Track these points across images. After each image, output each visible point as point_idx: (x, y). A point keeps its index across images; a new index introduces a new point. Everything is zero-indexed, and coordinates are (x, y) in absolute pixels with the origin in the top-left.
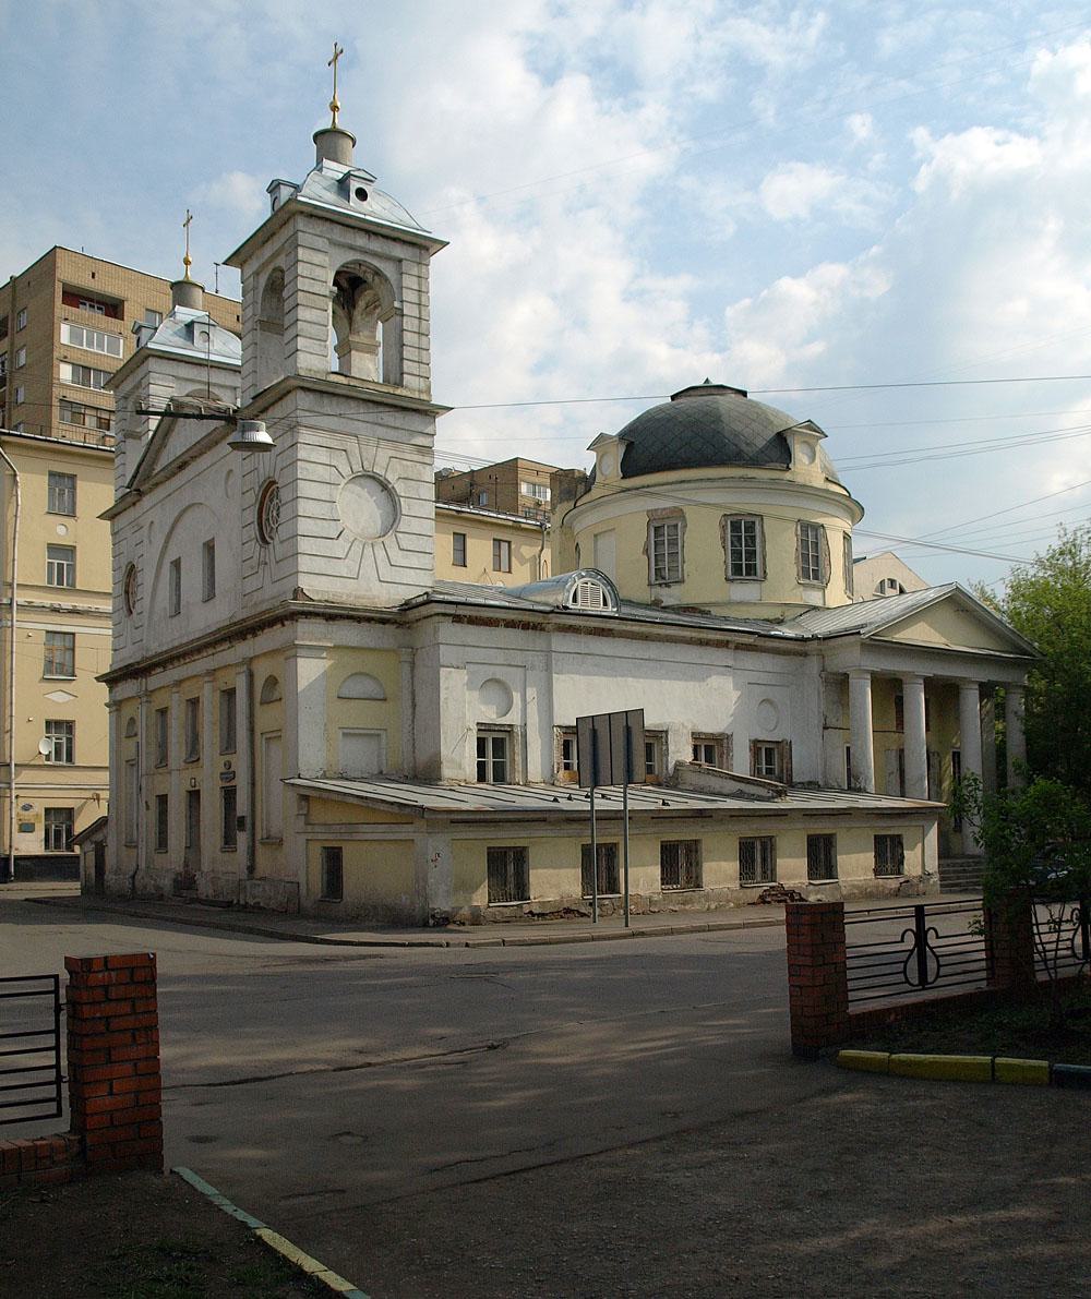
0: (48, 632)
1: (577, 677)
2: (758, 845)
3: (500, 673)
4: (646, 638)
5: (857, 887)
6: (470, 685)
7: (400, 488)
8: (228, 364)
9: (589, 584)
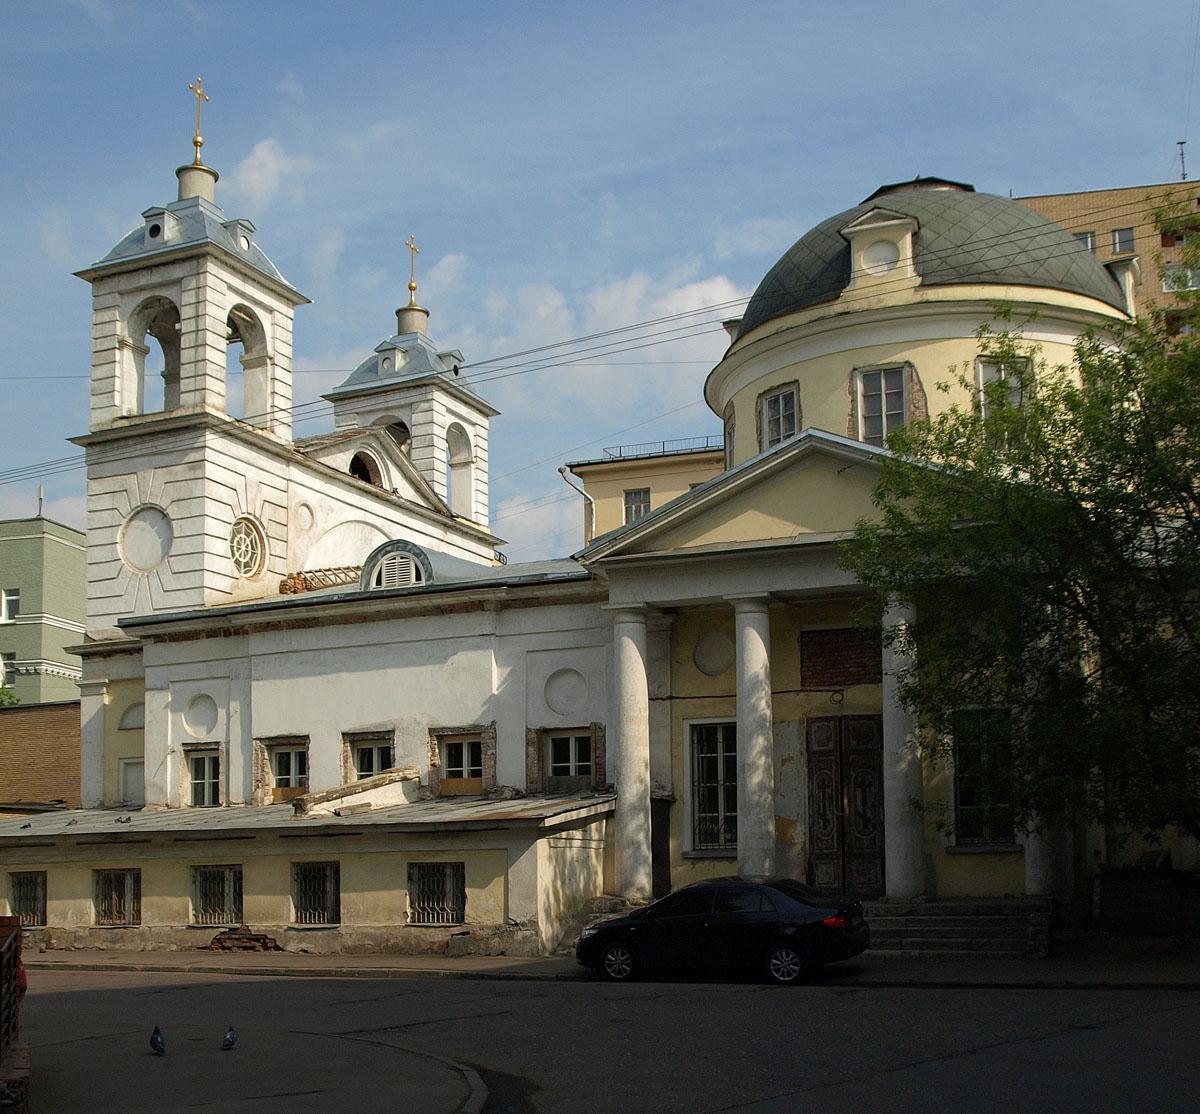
1: (278, 682)
2: (229, 875)
3: (205, 687)
4: (364, 619)
5: (371, 937)
6: (174, 707)
7: (172, 512)
8: (363, 390)
9: (398, 560)
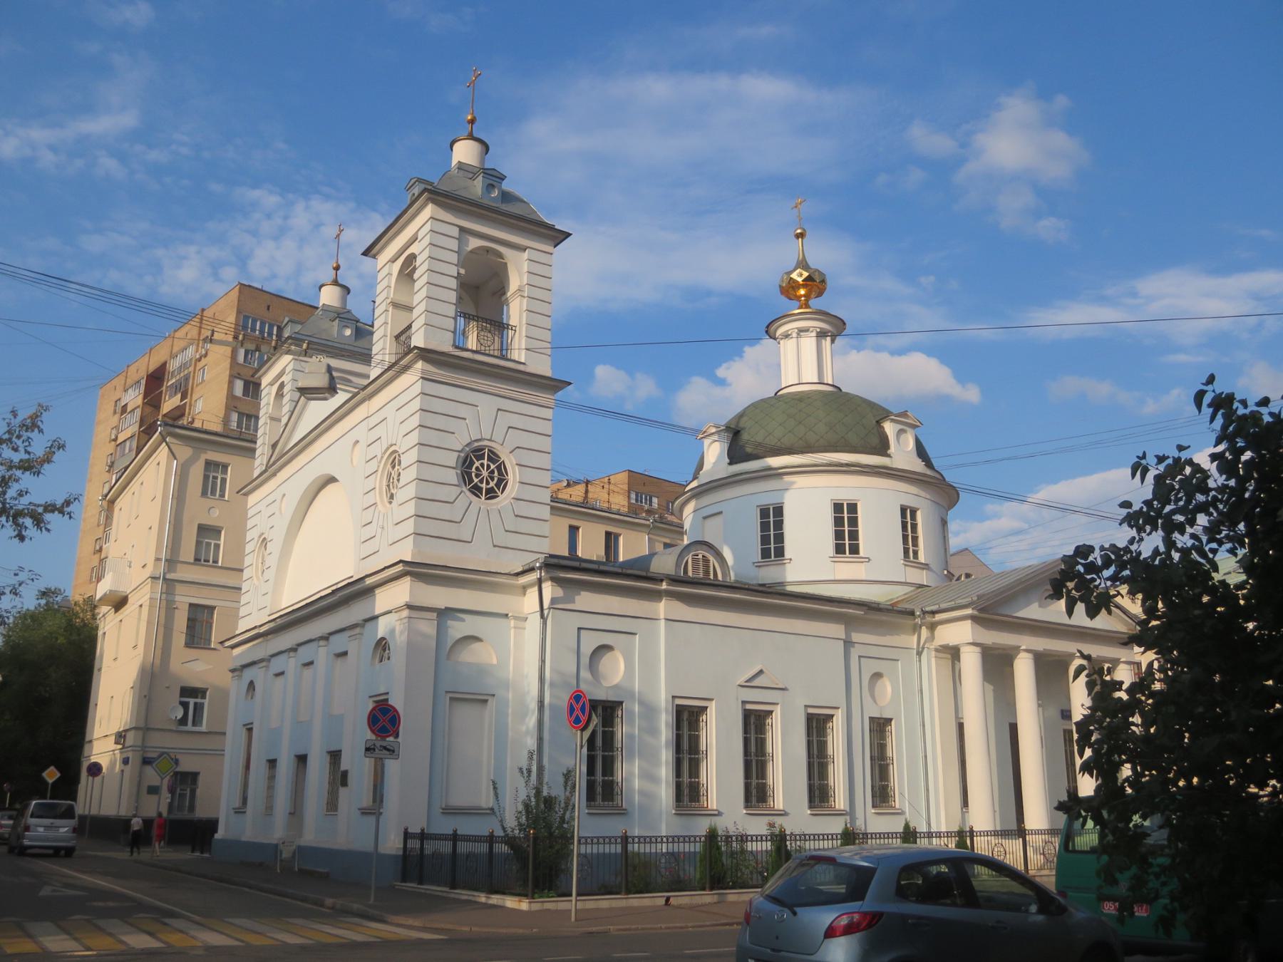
0: (191, 605)
